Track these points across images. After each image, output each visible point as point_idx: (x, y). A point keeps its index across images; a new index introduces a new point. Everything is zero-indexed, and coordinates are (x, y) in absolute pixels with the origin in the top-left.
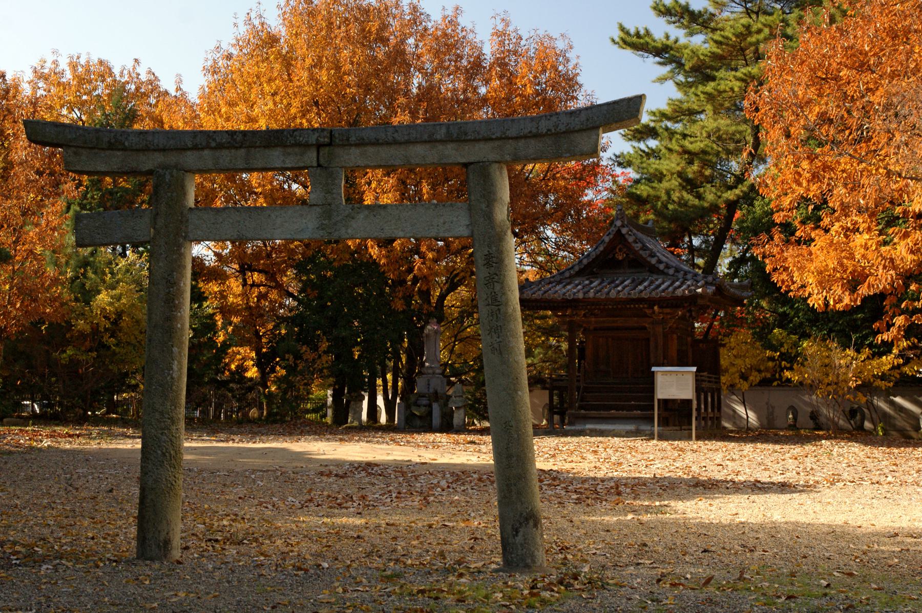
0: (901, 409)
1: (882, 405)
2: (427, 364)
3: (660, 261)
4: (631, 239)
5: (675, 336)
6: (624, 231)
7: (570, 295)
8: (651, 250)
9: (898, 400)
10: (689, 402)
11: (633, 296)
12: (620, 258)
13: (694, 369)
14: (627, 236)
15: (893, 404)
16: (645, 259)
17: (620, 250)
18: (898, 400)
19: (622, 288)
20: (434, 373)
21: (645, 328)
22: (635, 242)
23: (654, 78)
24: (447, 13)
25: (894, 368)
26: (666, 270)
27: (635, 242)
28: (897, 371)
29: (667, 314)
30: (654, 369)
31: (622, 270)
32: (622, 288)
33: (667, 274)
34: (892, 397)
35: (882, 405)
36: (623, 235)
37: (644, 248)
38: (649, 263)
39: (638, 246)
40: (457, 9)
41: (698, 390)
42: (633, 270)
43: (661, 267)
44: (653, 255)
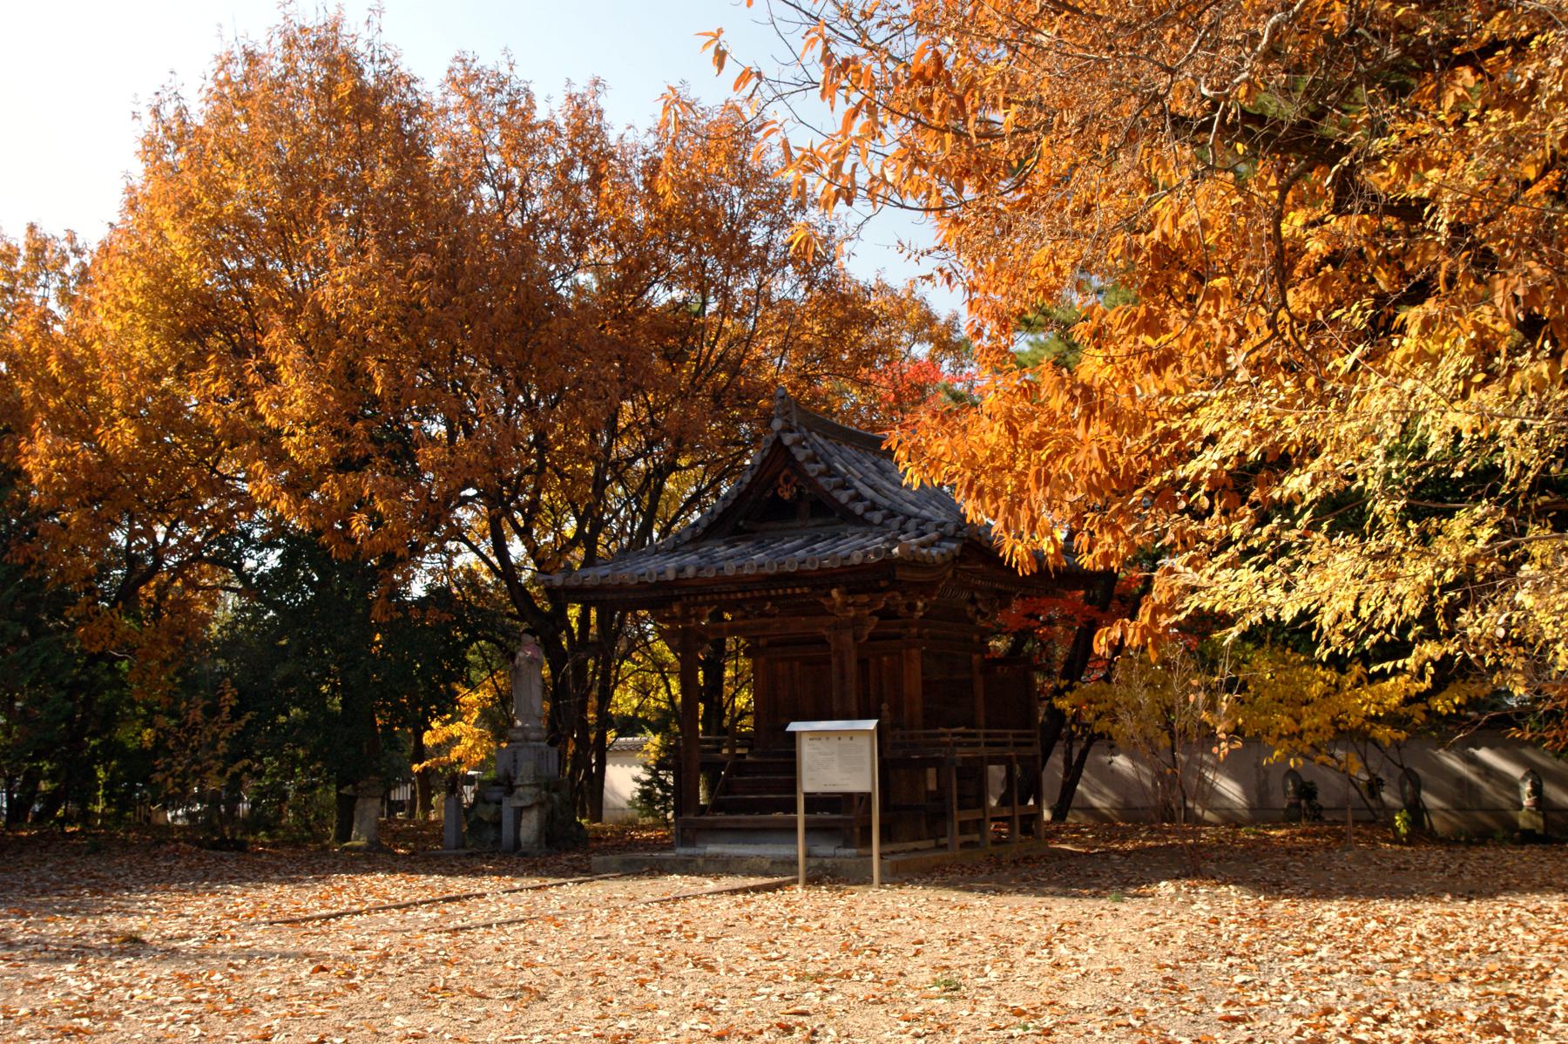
0: (1487, 771)
1: (1454, 763)
2: (519, 723)
3: (859, 497)
4: (800, 455)
5: (914, 652)
6: (788, 439)
7: (651, 575)
8: (843, 476)
9: (1484, 754)
10: (866, 798)
11: (787, 568)
12: (787, 496)
13: (871, 724)
14: (794, 450)
15: (1473, 761)
16: (829, 494)
17: (787, 480)
18: (1484, 754)
19: (795, 552)
20: (526, 739)
21: (822, 641)
22: (813, 459)
23: (716, 70)
24: (574, 91)
25: (1408, 700)
26: (868, 515)
27: (813, 459)
28: (1423, 706)
29: (864, 605)
30: (794, 726)
31: (798, 523)
32: (795, 552)
33: (869, 523)
34: (1472, 750)
35: (1454, 763)
36: (787, 448)
37: (830, 471)
38: (836, 500)
39: (813, 469)
40: (596, 83)
41: (886, 768)
42: (819, 521)
43: (859, 508)
44: (845, 485)
